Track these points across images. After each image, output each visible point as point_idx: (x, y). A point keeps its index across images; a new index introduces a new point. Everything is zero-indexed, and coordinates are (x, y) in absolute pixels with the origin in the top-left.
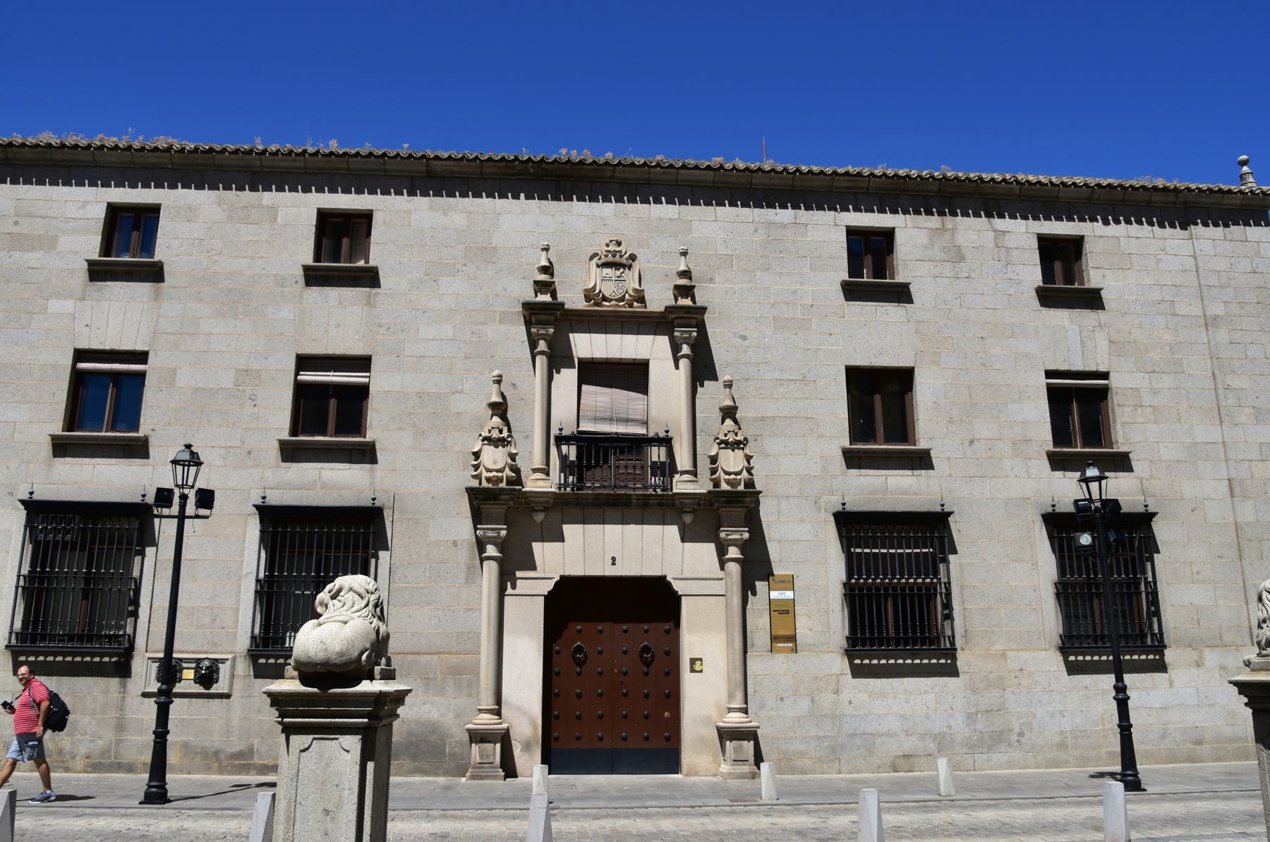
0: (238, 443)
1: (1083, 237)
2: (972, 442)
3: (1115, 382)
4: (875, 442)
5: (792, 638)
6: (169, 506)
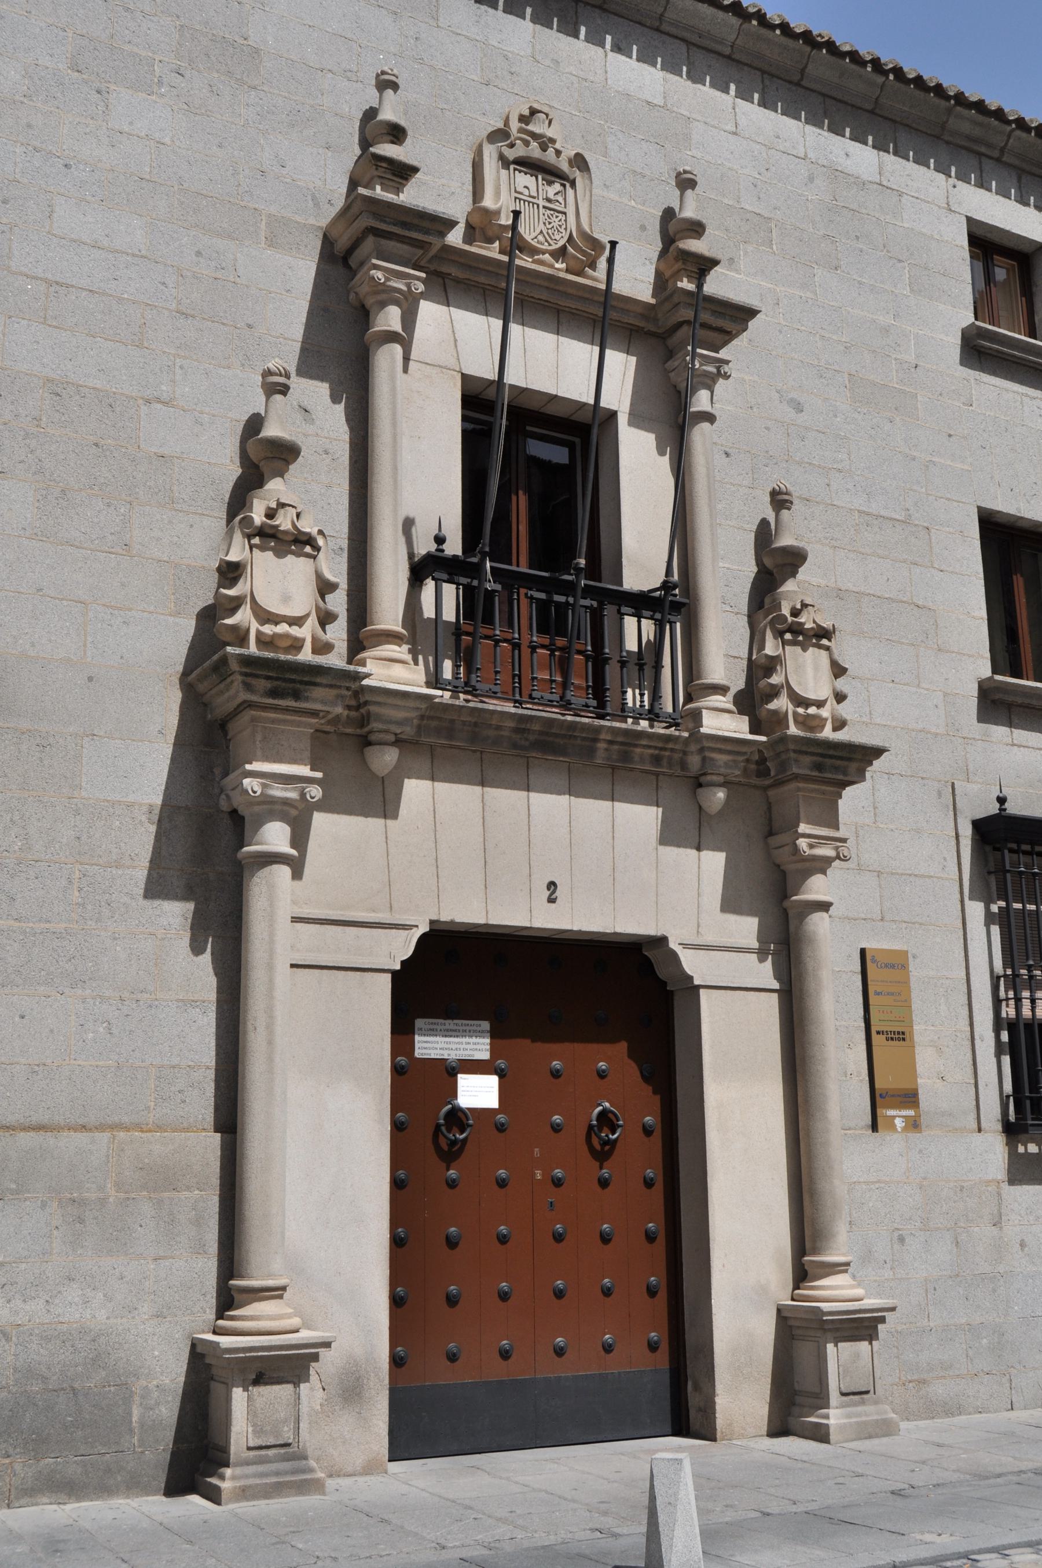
5: (909, 1098)
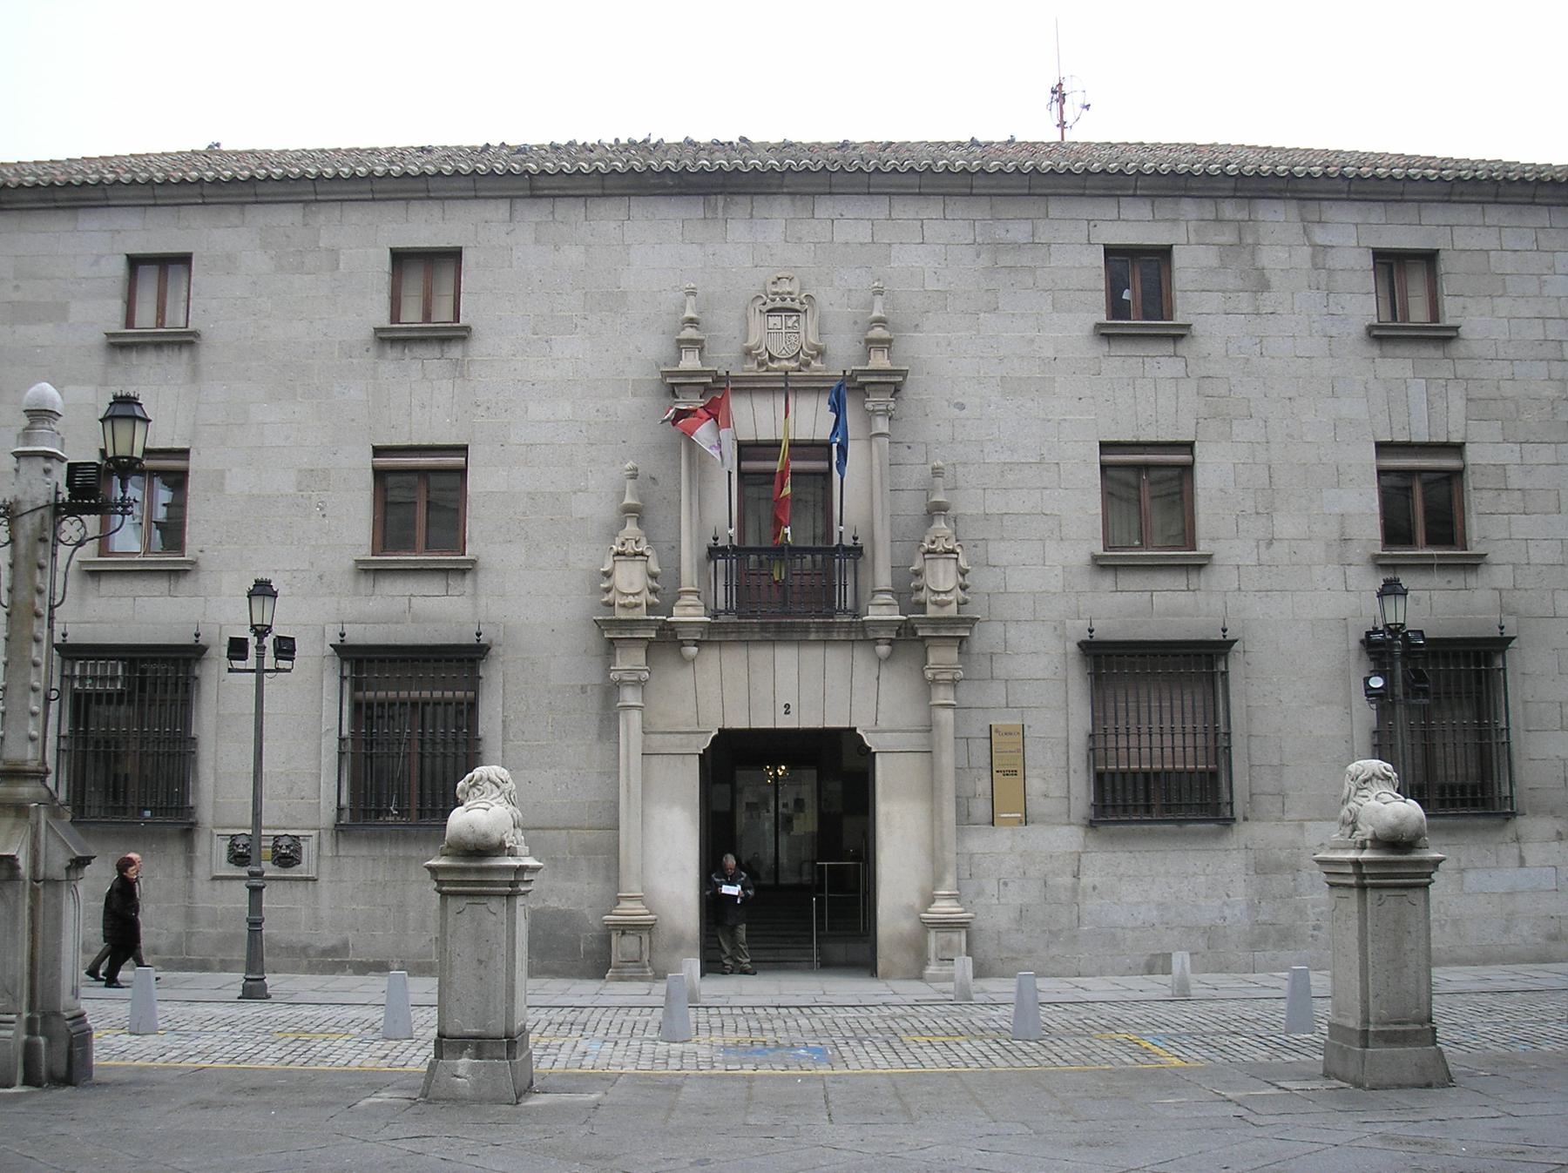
0: (306, 566)
2: (1270, 543)
3: (1474, 455)
6: (245, 658)
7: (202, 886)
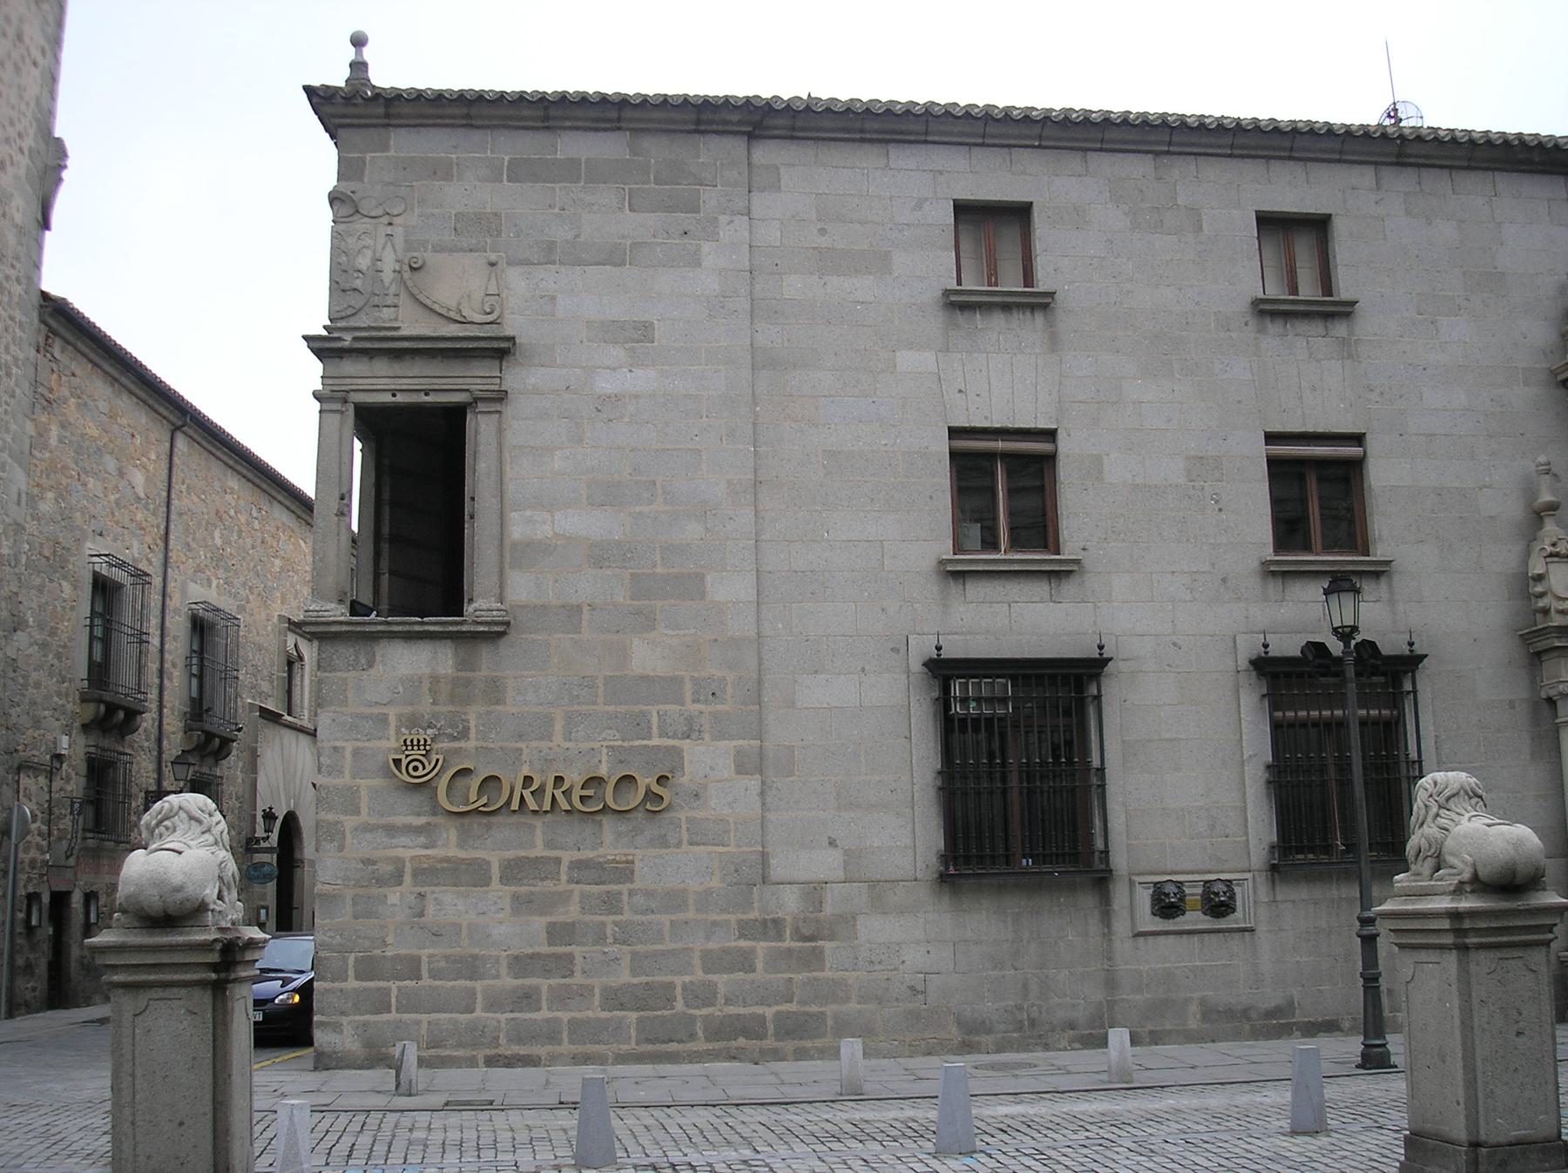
1: (1330, 215)
4: (1307, 547)
7: (1123, 944)
